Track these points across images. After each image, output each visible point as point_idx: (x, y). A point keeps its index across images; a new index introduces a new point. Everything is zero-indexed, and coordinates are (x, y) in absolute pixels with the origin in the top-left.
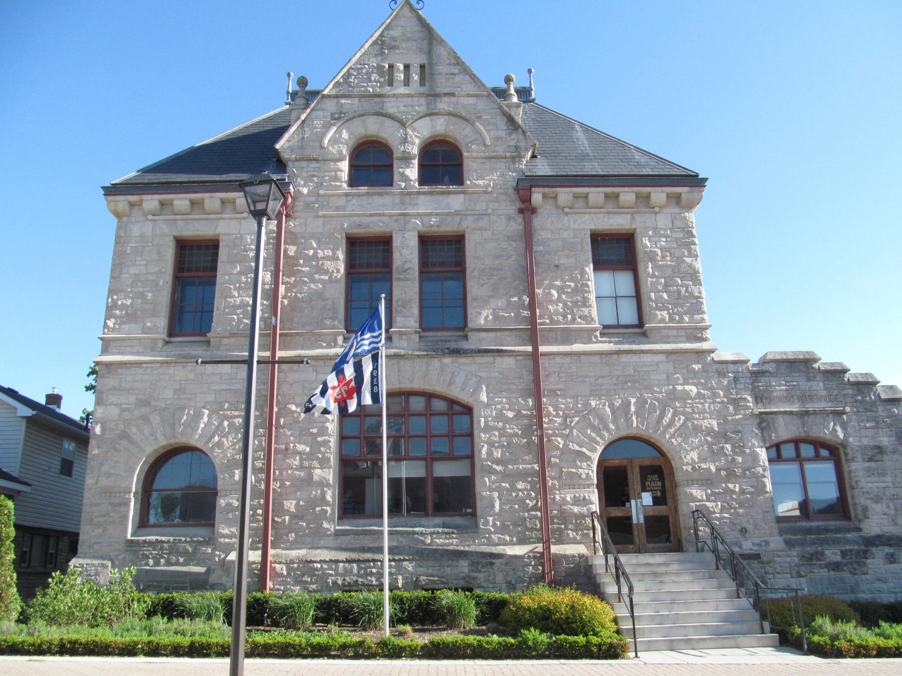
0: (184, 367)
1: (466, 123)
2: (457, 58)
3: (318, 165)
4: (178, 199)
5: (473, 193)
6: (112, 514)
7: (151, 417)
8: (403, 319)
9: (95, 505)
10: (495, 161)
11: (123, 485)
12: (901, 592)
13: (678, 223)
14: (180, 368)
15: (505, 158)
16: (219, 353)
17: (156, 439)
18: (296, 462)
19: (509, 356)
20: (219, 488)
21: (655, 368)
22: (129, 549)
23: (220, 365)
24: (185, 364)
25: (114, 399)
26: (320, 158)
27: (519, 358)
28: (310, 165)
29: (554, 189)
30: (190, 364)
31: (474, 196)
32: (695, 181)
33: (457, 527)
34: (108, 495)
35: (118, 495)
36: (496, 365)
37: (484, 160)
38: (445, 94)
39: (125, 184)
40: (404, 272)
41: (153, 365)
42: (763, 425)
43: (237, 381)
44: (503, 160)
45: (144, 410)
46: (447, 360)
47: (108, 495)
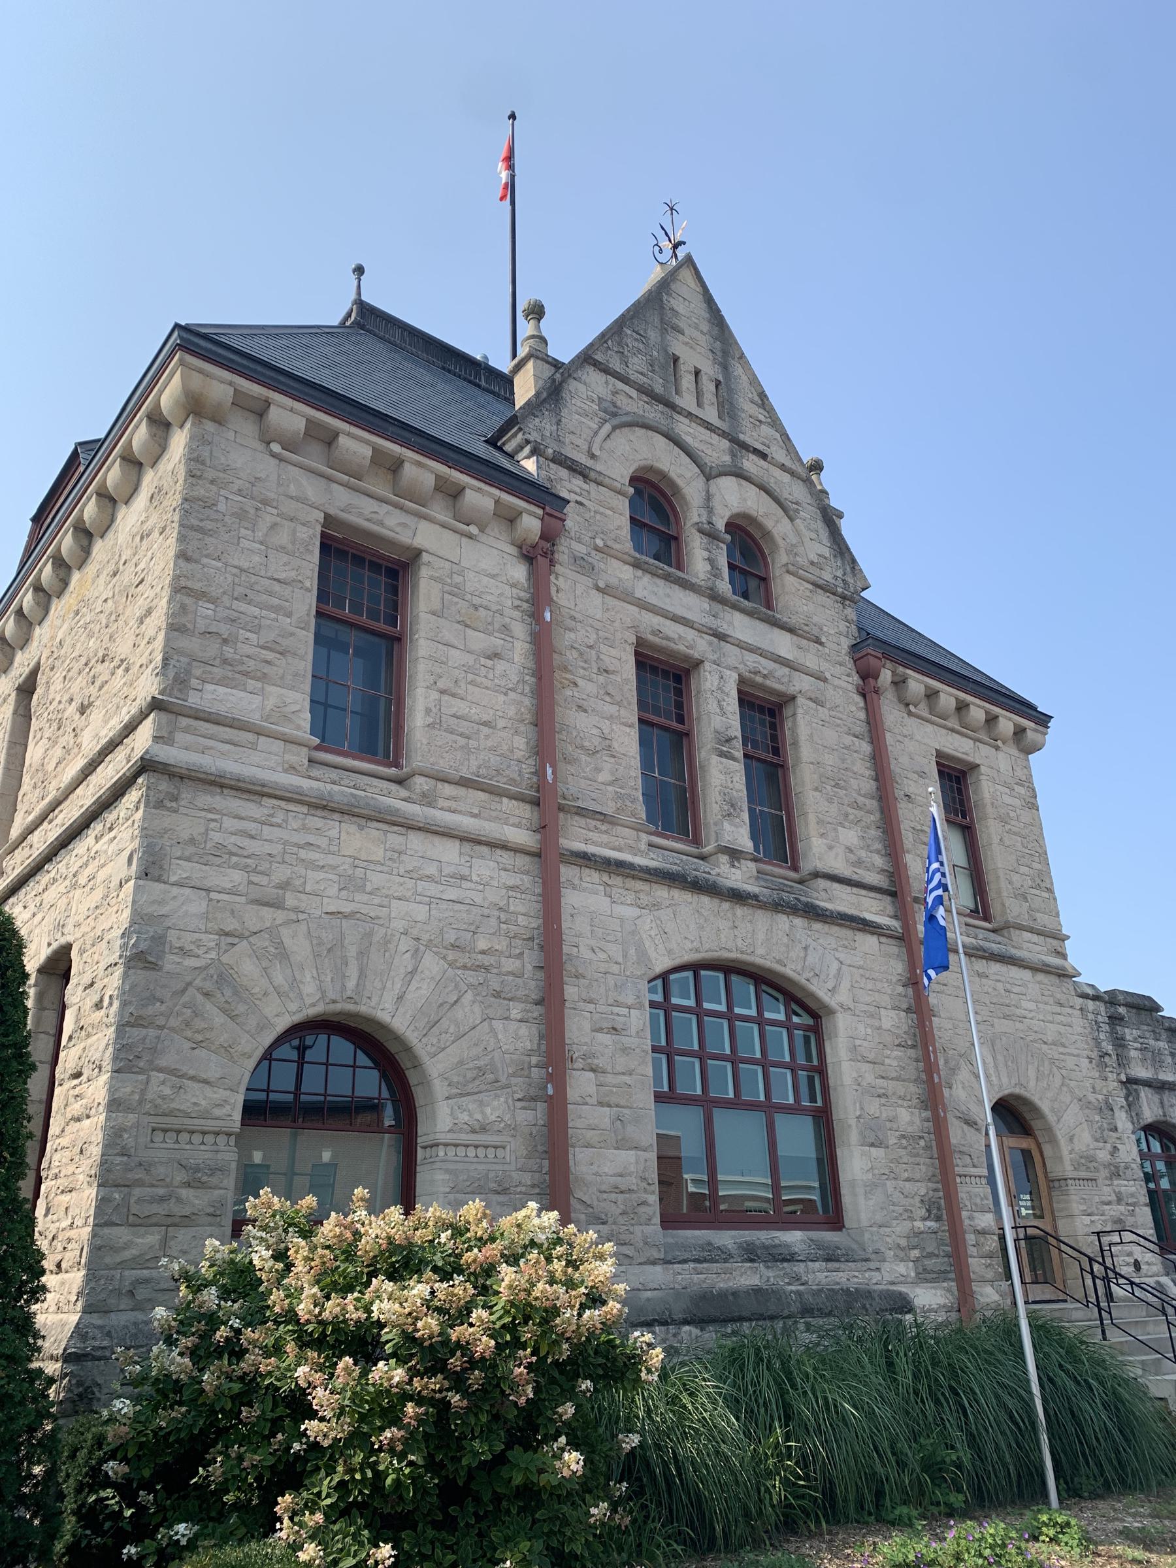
0: (361, 828)
2: (762, 395)
3: (586, 486)
4: (349, 434)
12: (1163, 1304)
13: (1020, 773)
14: (353, 828)
15: (834, 594)
18: (992, 1531)
19: (873, 934)
23: (437, 840)
24: (363, 822)
26: (593, 475)
30: (376, 825)
32: (1043, 720)
33: (225, 778)
38: (755, 449)
39: (204, 337)
41: (291, 807)
42: (1131, 1099)
43: (473, 886)
46: (798, 922)
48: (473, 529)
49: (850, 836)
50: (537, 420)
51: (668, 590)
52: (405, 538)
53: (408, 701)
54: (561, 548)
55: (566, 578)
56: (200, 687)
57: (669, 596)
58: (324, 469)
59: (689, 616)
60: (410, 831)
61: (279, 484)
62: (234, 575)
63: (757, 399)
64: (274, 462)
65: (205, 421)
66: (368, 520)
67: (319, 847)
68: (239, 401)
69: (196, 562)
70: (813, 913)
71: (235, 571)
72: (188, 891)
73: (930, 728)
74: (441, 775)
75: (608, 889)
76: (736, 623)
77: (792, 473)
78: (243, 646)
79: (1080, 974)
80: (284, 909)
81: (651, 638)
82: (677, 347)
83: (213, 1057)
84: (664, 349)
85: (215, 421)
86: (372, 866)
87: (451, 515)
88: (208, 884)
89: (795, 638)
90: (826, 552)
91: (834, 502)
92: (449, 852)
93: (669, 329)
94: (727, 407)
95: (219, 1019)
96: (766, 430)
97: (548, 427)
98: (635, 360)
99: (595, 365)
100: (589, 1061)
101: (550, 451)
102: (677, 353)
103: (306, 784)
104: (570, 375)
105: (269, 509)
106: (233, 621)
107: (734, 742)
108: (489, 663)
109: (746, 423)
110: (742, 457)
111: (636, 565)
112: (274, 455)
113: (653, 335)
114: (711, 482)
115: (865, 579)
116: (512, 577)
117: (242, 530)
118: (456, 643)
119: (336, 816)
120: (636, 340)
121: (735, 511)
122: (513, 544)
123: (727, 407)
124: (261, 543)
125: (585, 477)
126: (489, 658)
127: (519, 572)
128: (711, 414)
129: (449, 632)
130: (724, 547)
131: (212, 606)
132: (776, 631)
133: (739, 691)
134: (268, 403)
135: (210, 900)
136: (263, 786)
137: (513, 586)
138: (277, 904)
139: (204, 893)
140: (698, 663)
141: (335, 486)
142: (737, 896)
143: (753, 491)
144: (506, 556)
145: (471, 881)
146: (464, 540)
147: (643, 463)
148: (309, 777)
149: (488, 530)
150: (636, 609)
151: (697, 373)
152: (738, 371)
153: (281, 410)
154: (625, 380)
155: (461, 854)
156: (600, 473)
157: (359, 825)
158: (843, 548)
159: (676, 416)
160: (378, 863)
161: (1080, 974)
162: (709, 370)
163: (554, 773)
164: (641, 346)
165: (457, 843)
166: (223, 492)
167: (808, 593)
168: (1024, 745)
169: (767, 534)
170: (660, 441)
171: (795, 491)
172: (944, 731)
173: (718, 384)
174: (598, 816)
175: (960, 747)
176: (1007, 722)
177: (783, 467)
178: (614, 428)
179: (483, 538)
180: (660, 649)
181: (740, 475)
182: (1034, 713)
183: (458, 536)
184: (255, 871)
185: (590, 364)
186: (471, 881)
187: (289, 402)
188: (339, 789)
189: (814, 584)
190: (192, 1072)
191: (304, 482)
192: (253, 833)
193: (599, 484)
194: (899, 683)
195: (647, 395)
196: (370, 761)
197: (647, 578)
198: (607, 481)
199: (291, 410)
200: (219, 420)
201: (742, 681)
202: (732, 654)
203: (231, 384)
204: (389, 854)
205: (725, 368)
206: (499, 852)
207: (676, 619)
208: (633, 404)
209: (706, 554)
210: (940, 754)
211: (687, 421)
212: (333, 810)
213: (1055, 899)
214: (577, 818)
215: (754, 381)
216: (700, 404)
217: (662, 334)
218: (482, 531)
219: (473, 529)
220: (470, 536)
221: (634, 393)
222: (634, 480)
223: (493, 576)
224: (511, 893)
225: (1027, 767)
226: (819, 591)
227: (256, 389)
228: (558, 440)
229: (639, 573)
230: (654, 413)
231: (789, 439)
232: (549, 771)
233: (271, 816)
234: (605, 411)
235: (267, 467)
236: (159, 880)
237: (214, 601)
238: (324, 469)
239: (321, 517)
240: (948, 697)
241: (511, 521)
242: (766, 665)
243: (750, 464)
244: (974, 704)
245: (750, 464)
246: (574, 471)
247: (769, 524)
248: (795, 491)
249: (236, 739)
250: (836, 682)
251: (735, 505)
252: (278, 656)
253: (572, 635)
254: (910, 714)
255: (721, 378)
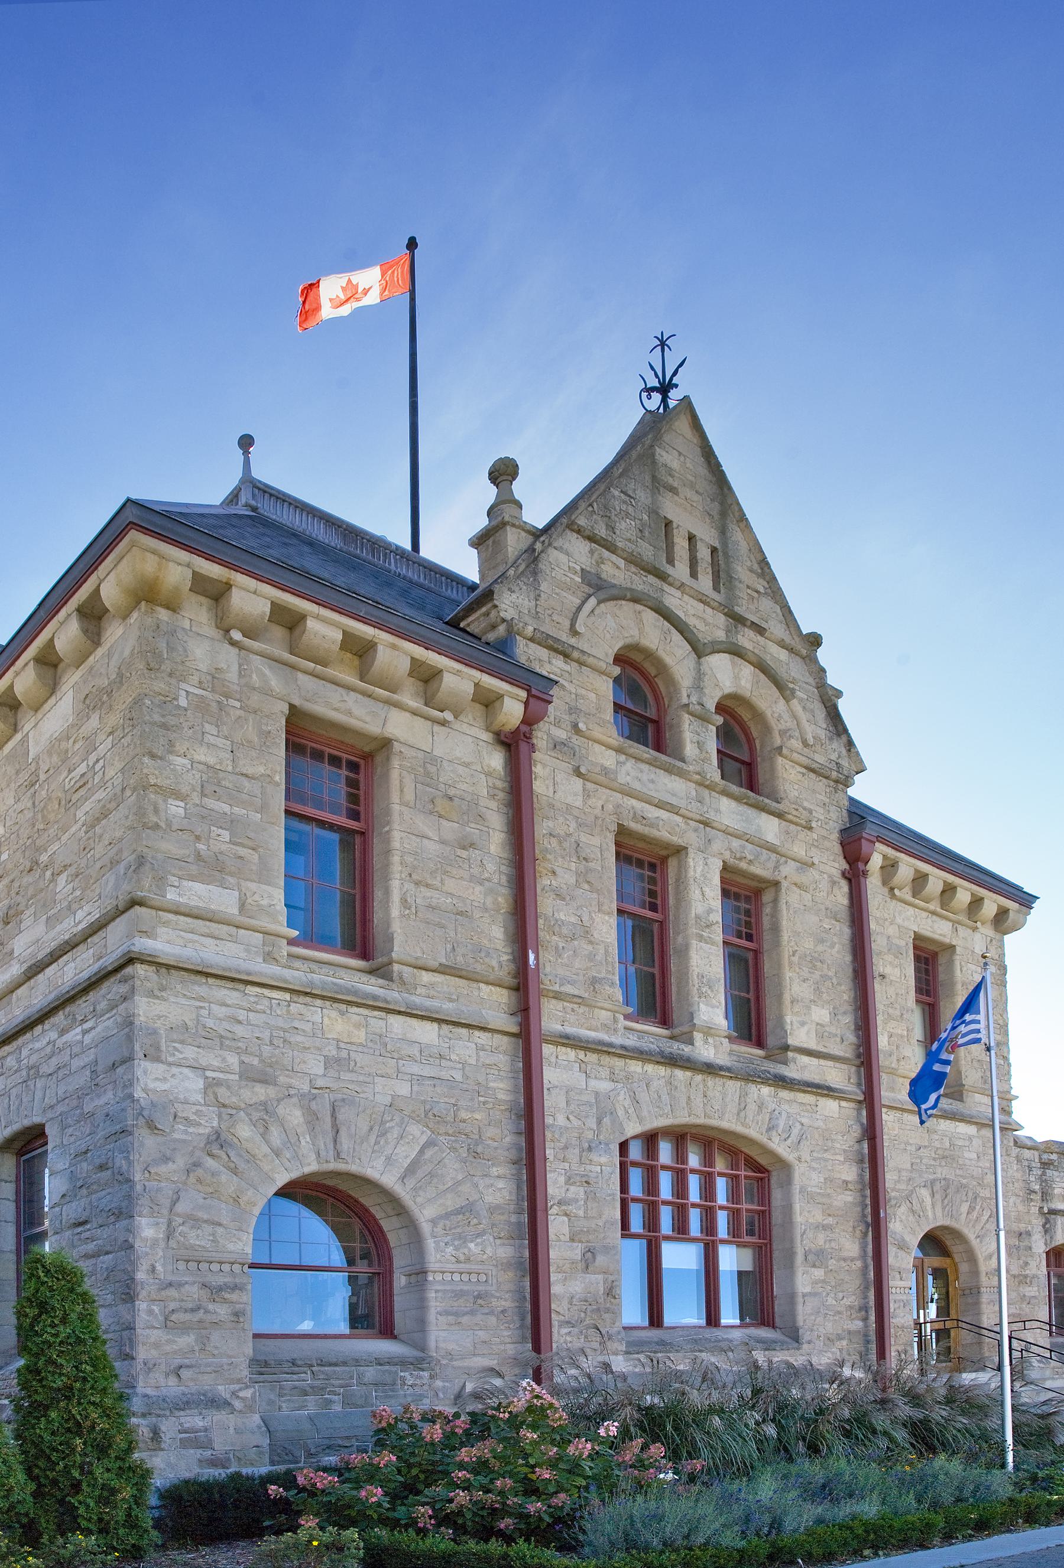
0: (342, 1013)
1: (777, 693)
2: (764, 563)
3: (567, 668)
4: (317, 617)
5: (791, 822)
6: (211, 1307)
7: (281, 1110)
8: (710, 1009)
9: (170, 1285)
10: (409, 743)
11: (231, 1247)
14: (334, 1014)
15: (826, 778)
16: (417, 1000)
17: (296, 1156)
20: (800, 1323)
21: (967, 1143)
22: (262, 1378)
24: (343, 1007)
25: (190, 1053)
26: (575, 654)
27: (844, 1104)
28: (554, 661)
29: (898, 854)
30: (355, 1010)
31: (792, 827)
32: (1026, 901)
34: (192, 1265)
35: (226, 1267)
36: (818, 1109)
37: (804, 771)
40: (707, 926)
44: (824, 780)
45: (261, 1092)
47: (192, 1265)
48: (448, 715)
49: (821, 1014)
50: (514, 596)
51: (653, 776)
52: (373, 728)
53: (378, 894)
54: (539, 734)
55: (544, 766)
56: (176, 884)
57: (652, 781)
58: (286, 656)
59: (674, 801)
60: (389, 1016)
61: (240, 675)
62: (201, 772)
63: (756, 567)
64: (234, 651)
65: (159, 609)
66: (335, 709)
67: (304, 1031)
68: (200, 585)
69: (161, 758)
70: (782, 1082)
71: (201, 767)
72: (186, 1071)
73: (911, 911)
74: (420, 963)
75: (583, 1065)
76: (723, 808)
77: (791, 650)
78: (216, 842)
79: (1022, 1127)
80: (276, 1085)
81: (634, 826)
82: (670, 508)
83: (223, 1206)
84: (654, 512)
85: (168, 608)
86: (354, 1048)
87: (423, 702)
88: (204, 1062)
89: (784, 823)
90: (822, 734)
91: (832, 680)
92: (427, 1033)
93: (661, 489)
94: (721, 576)
95: (225, 1177)
96: (767, 605)
97: (526, 602)
98: (623, 525)
99: (578, 532)
100: (564, 1207)
101: (530, 629)
102: (669, 517)
103: (287, 973)
104: (550, 545)
105: (232, 702)
106: (203, 817)
107: (715, 927)
108: (464, 854)
109: (743, 593)
110: (737, 632)
111: (619, 750)
112: (233, 643)
113: (643, 496)
114: (703, 660)
115: (862, 761)
116: (489, 766)
117: (207, 725)
118: (431, 834)
119: (319, 1002)
120: (625, 502)
121: (727, 691)
122: (488, 729)
123: (721, 576)
124: (226, 738)
125: (566, 656)
126: (464, 848)
127: (496, 760)
128: (705, 583)
129: (422, 824)
130: (714, 729)
131: (182, 804)
132: (764, 815)
133: (723, 880)
134: (228, 586)
135: (207, 1078)
136: (249, 974)
137: (488, 774)
138: (265, 1080)
139: (200, 1072)
140: (680, 851)
141: (300, 675)
142: (710, 1069)
143: (747, 671)
144: (481, 743)
145: (450, 1060)
146: (437, 728)
147: (629, 641)
148: (290, 967)
149: (461, 717)
150: (619, 796)
151: (691, 538)
152: (737, 535)
153: (243, 593)
154: (611, 548)
155: (439, 1035)
156: (582, 652)
157: (340, 1011)
158: (840, 728)
159: (666, 587)
160: (361, 1045)
161: (1022, 1127)
162: (707, 535)
163: (537, 958)
164: (631, 510)
165: (435, 1025)
166: (183, 686)
167: (800, 776)
168: (1002, 922)
169: (758, 716)
170: (649, 616)
171: (792, 669)
172: (924, 914)
173: (714, 550)
174: (575, 1000)
175: (939, 930)
176: (991, 904)
177: (782, 644)
178: (599, 603)
179: (457, 725)
180: (642, 838)
181: (736, 652)
182: (1021, 895)
183: (430, 723)
184: (246, 1051)
185: (573, 530)
186: (450, 1060)
187: (252, 583)
188: (321, 978)
189: (806, 768)
190: (205, 1217)
191: (267, 672)
192: (241, 1018)
193: (581, 664)
194: (890, 868)
195: (636, 565)
196: (327, 952)
197: (630, 764)
198: (590, 660)
199: (255, 593)
200: (172, 607)
201: (726, 868)
202: (719, 844)
203: (188, 566)
204: (371, 1037)
205: (723, 532)
206: (477, 1033)
207: (661, 805)
208: (616, 571)
209: (696, 738)
210: (918, 938)
211: (678, 594)
212: (315, 996)
213: (1009, 1065)
214: (554, 1001)
215: (757, 548)
216: (694, 574)
217: (653, 495)
218: (456, 717)
219: (448, 715)
220: (443, 723)
221: (622, 563)
222: (618, 659)
223: (467, 765)
224: (488, 1071)
225: (1001, 946)
226: (812, 775)
227: (214, 570)
228: (536, 616)
229: (623, 758)
230: (643, 583)
231: (790, 612)
232: (532, 957)
233: (256, 1003)
234: (589, 585)
235: (229, 656)
236: (158, 1060)
237: (183, 798)
238: (286, 656)
239: (286, 709)
240: (937, 879)
241: (487, 706)
242: (749, 851)
243: (746, 639)
244: (962, 887)
245: (746, 639)
246: (556, 651)
247: (762, 704)
248: (792, 669)
249: (216, 933)
250: (822, 867)
251: (728, 684)
252: (250, 851)
253: (551, 824)
254: (893, 896)
255: (717, 544)
